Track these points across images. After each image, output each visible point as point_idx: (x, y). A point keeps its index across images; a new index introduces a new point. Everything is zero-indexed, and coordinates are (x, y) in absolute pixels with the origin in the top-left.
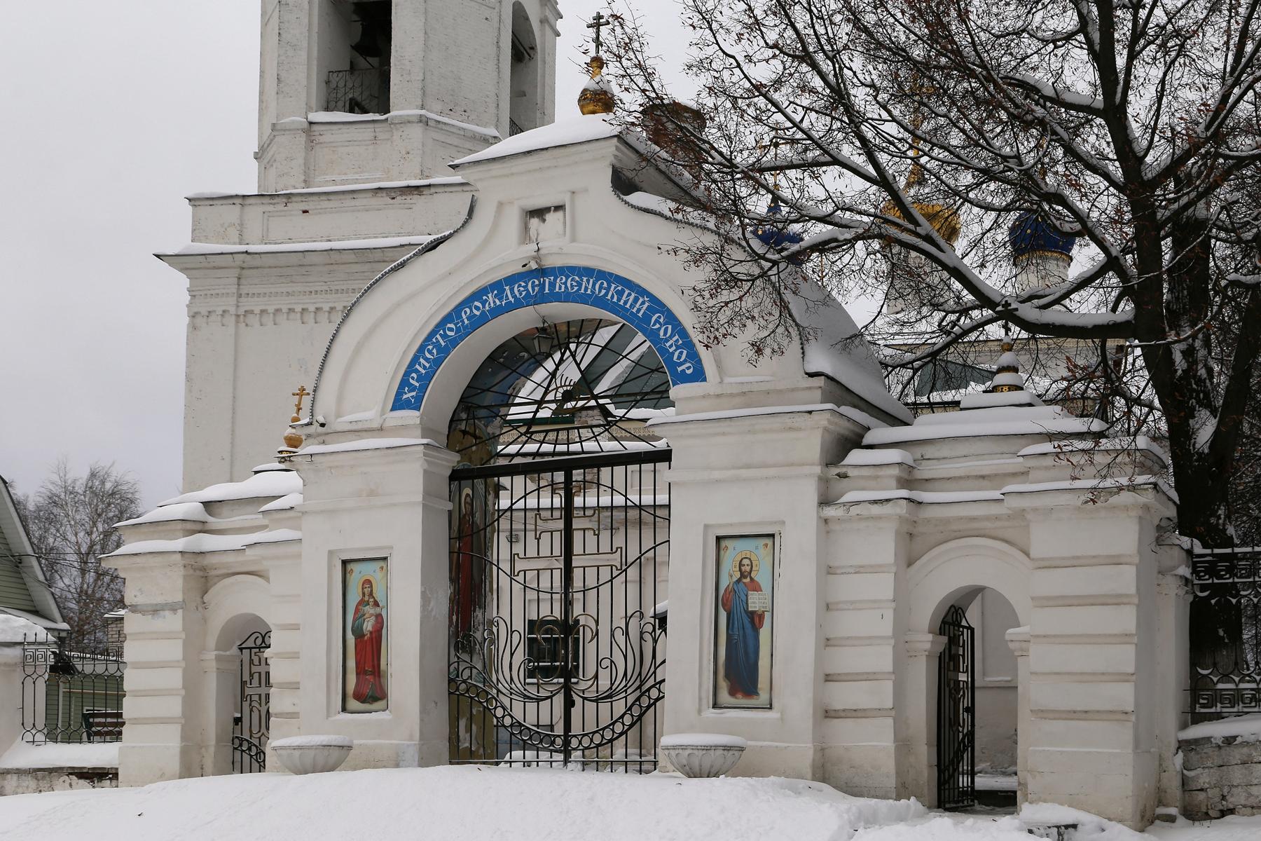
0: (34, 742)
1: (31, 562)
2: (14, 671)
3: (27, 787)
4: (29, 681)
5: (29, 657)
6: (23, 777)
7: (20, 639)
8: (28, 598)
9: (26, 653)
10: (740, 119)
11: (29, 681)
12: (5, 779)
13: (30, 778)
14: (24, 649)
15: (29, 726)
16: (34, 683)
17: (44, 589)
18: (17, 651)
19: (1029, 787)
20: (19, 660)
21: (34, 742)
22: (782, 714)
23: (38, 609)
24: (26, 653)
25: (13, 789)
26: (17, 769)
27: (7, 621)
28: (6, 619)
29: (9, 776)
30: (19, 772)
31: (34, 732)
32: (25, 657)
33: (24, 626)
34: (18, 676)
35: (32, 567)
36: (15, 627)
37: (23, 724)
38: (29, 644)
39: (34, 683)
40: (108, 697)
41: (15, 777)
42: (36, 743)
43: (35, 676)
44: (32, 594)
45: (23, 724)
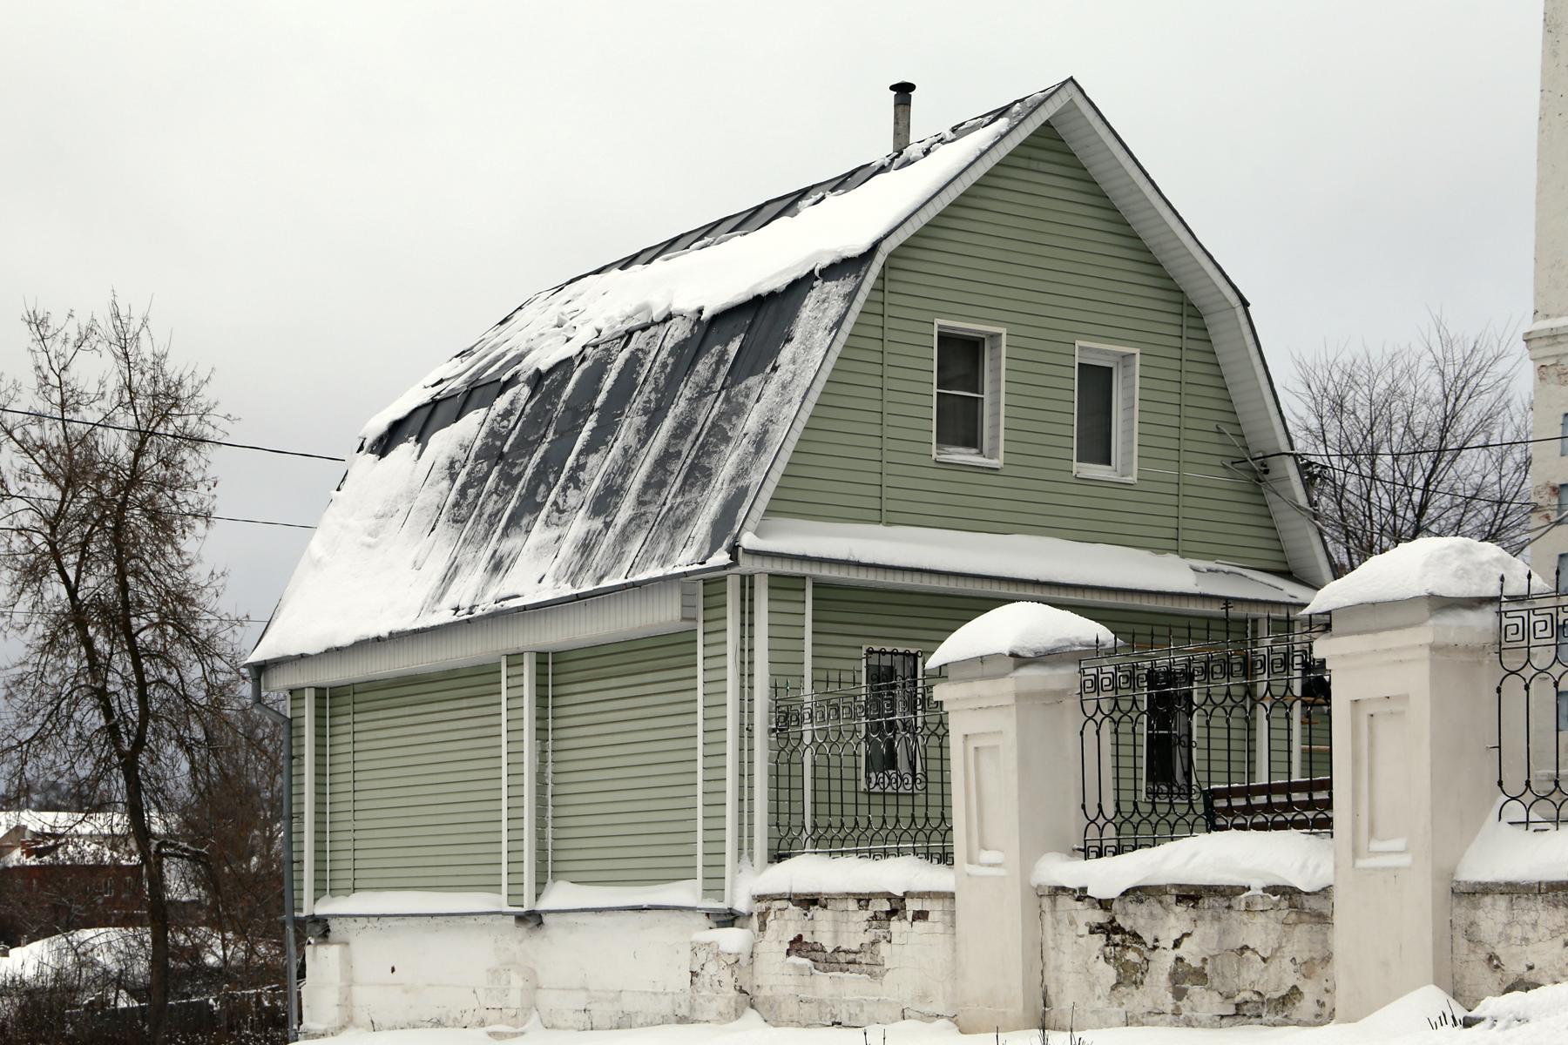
0: (1527, 823)
1: (1285, 469)
2: (1480, 663)
3: (1535, 925)
4: (1514, 686)
5: (1540, 626)
6: (1523, 902)
7: (1492, 590)
8: (1275, 545)
9: (1505, 621)
10: (38, 682)
11: (1514, 686)
12: (1476, 907)
13: (1540, 905)
14: (1499, 613)
15: (1515, 784)
16: (1527, 687)
17: (1307, 524)
18: (1484, 620)
19: (321, 949)
20: (1490, 639)
21: (1527, 823)
22: (1354, 864)
23: (1291, 566)
24: (1505, 621)
25: (1500, 928)
26: (1508, 884)
27: (1465, 551)
28: (1466, 545)
29: (1488, 900)
30: (1513, 890)
31: (1529, 798)
32: (1503, 630)
33: (1497, 560)
34: (1489, 675)
35: (1288, 478)
36: (1482, 564)
37: (1500, 783)
38: (1514, 599)
39: (1527, 687)
40: (1314, 757)
41: (1502, 902)
42: (1532, 827)
43: (1528, 672)
44: (1283, 536)
45: (1500, 783)
